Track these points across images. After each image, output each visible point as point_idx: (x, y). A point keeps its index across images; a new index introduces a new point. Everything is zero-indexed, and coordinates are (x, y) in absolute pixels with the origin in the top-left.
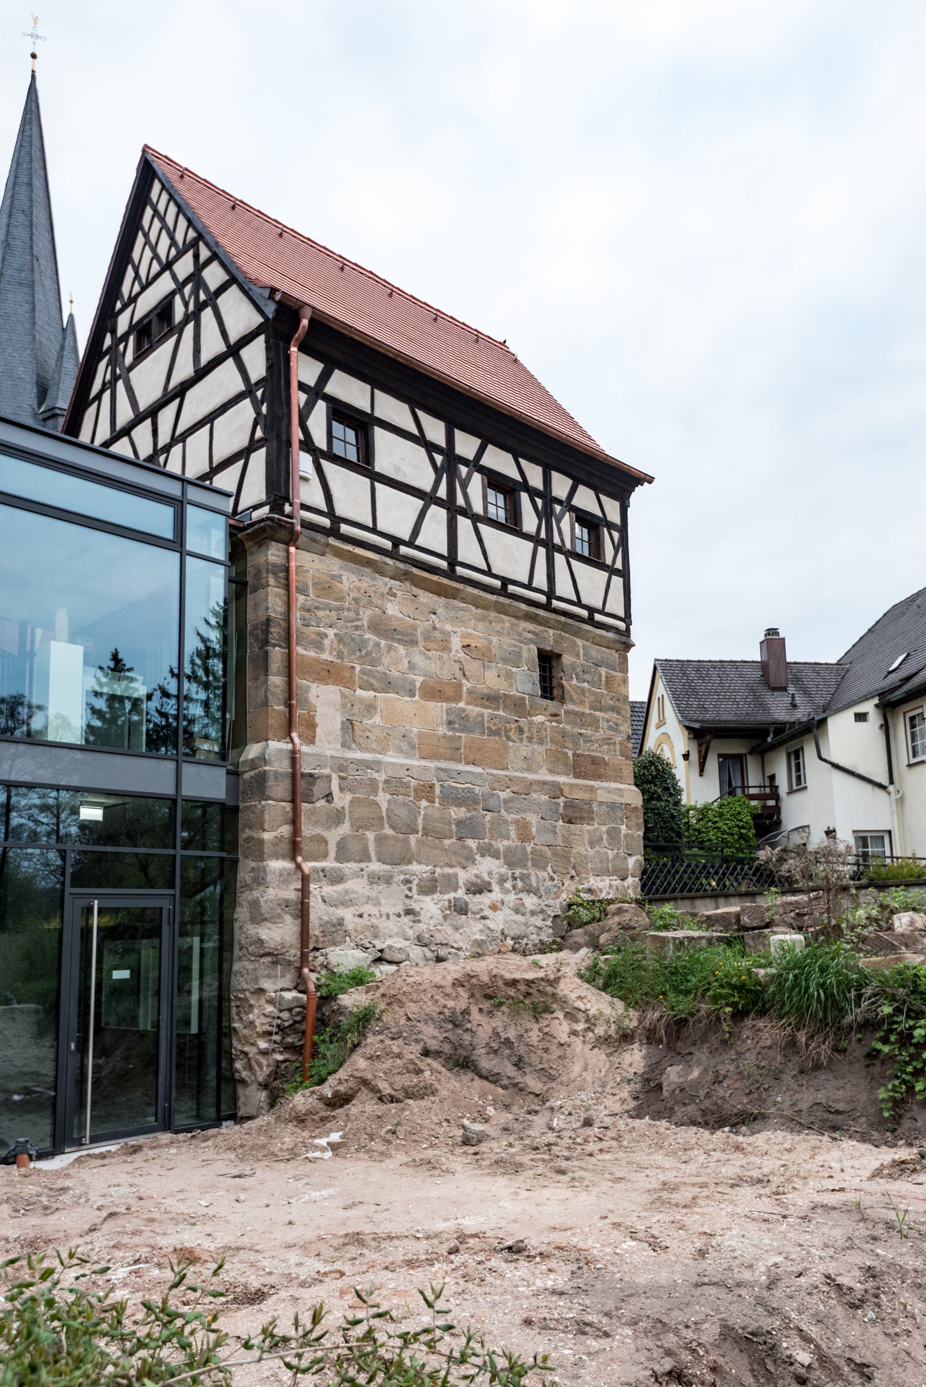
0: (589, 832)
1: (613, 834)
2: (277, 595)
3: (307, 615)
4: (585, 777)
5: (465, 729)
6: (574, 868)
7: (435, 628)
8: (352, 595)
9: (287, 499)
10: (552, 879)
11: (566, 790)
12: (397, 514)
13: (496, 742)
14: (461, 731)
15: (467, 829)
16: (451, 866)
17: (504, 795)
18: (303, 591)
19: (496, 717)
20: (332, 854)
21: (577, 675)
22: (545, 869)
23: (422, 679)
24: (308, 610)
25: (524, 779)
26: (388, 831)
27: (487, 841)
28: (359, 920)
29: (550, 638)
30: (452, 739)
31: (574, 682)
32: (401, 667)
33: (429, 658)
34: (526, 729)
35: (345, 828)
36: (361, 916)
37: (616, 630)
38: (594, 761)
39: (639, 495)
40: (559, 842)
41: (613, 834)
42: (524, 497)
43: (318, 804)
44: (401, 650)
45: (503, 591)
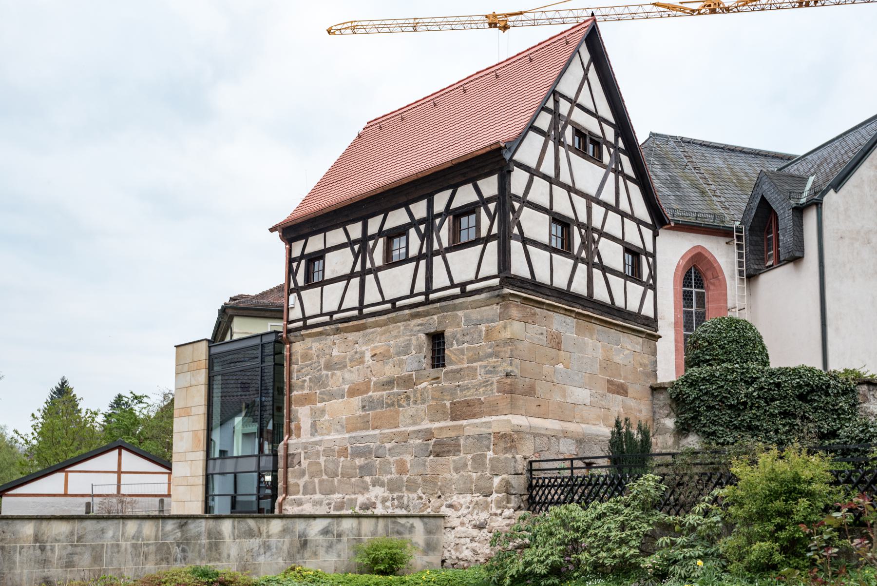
0: (454, 461)
1: (478, 462)
4: (460, 419)
5: (372, 408)
6: (440, 489)
11: (435, 432)
15: (366, 470)
16: (355, 494)
21: (457, 341)
22: (415, 491)
23: (348, 386)
26: (325, 477)
29: (433, 323)
30: (364, 416)
31: (455, 346)
34: (412, 396)
35: (306, 478)
38: (468, 404)
40: (428, 471)
41: (478, 462)
44: (338, 373)
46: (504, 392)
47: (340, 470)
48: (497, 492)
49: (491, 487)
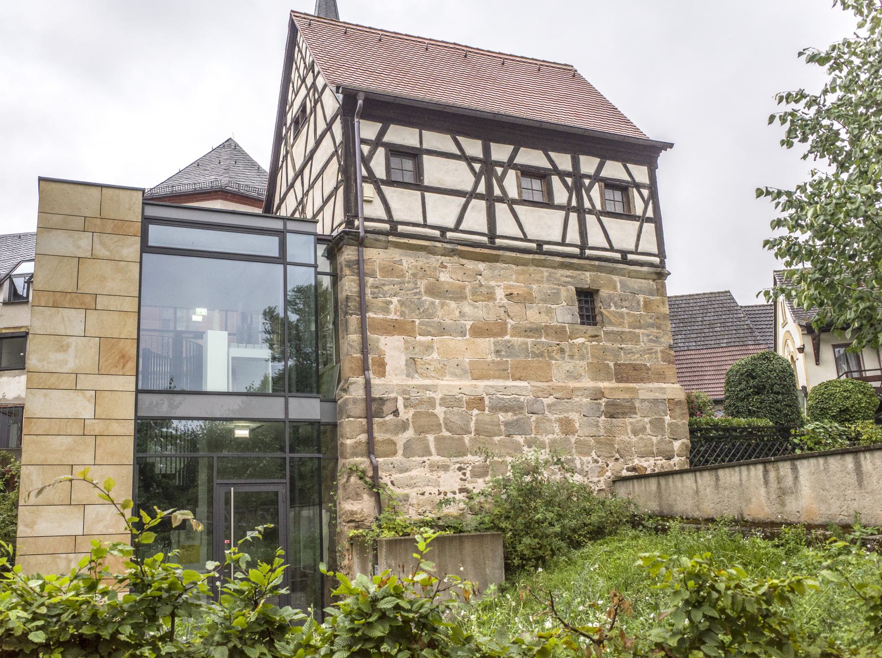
0: (631, 423)
1: (657, 424)
2: (352, 281)
3: (376, 290)
4: (627, 381)
6: (618, 452)
7: (481, 285)
8: (410, 272)
9: (356, 216)
10: (596, 461)
11: (606, 392)
12: (443, 211)
13: (540, 362)
14: (508, 357)
15: (513, 428)
17: (547, 401)
18: (373, 275)
19: (539, 343)
20: (400, 452)
22: (589, 454)
23: (471, 323)
24: (377, 287)
25: (565, 388)
27: (533, 436)
28: (421, 497)
29: (587, 279)
30: (499, 363)
31: (613, 308)
32: (453, 316)
33: (477, 307)
34: (567, 350)
35: (410, 433)
36: (423, 494)
37: (651, 265)
38: (635, 368)
39: (663, 158)
40: (602, 432)
41: (657, 424)
42: (555, 179)
43: (387, 418)
44: (453, 304)
45: (540, 251)
46: (670, 362)
47: (472, 425)
48: (678, 456)
49: (673, 451)
